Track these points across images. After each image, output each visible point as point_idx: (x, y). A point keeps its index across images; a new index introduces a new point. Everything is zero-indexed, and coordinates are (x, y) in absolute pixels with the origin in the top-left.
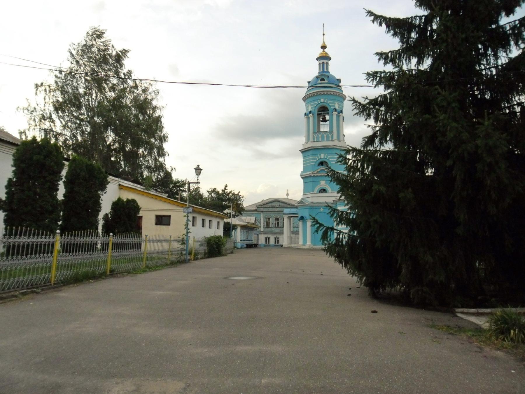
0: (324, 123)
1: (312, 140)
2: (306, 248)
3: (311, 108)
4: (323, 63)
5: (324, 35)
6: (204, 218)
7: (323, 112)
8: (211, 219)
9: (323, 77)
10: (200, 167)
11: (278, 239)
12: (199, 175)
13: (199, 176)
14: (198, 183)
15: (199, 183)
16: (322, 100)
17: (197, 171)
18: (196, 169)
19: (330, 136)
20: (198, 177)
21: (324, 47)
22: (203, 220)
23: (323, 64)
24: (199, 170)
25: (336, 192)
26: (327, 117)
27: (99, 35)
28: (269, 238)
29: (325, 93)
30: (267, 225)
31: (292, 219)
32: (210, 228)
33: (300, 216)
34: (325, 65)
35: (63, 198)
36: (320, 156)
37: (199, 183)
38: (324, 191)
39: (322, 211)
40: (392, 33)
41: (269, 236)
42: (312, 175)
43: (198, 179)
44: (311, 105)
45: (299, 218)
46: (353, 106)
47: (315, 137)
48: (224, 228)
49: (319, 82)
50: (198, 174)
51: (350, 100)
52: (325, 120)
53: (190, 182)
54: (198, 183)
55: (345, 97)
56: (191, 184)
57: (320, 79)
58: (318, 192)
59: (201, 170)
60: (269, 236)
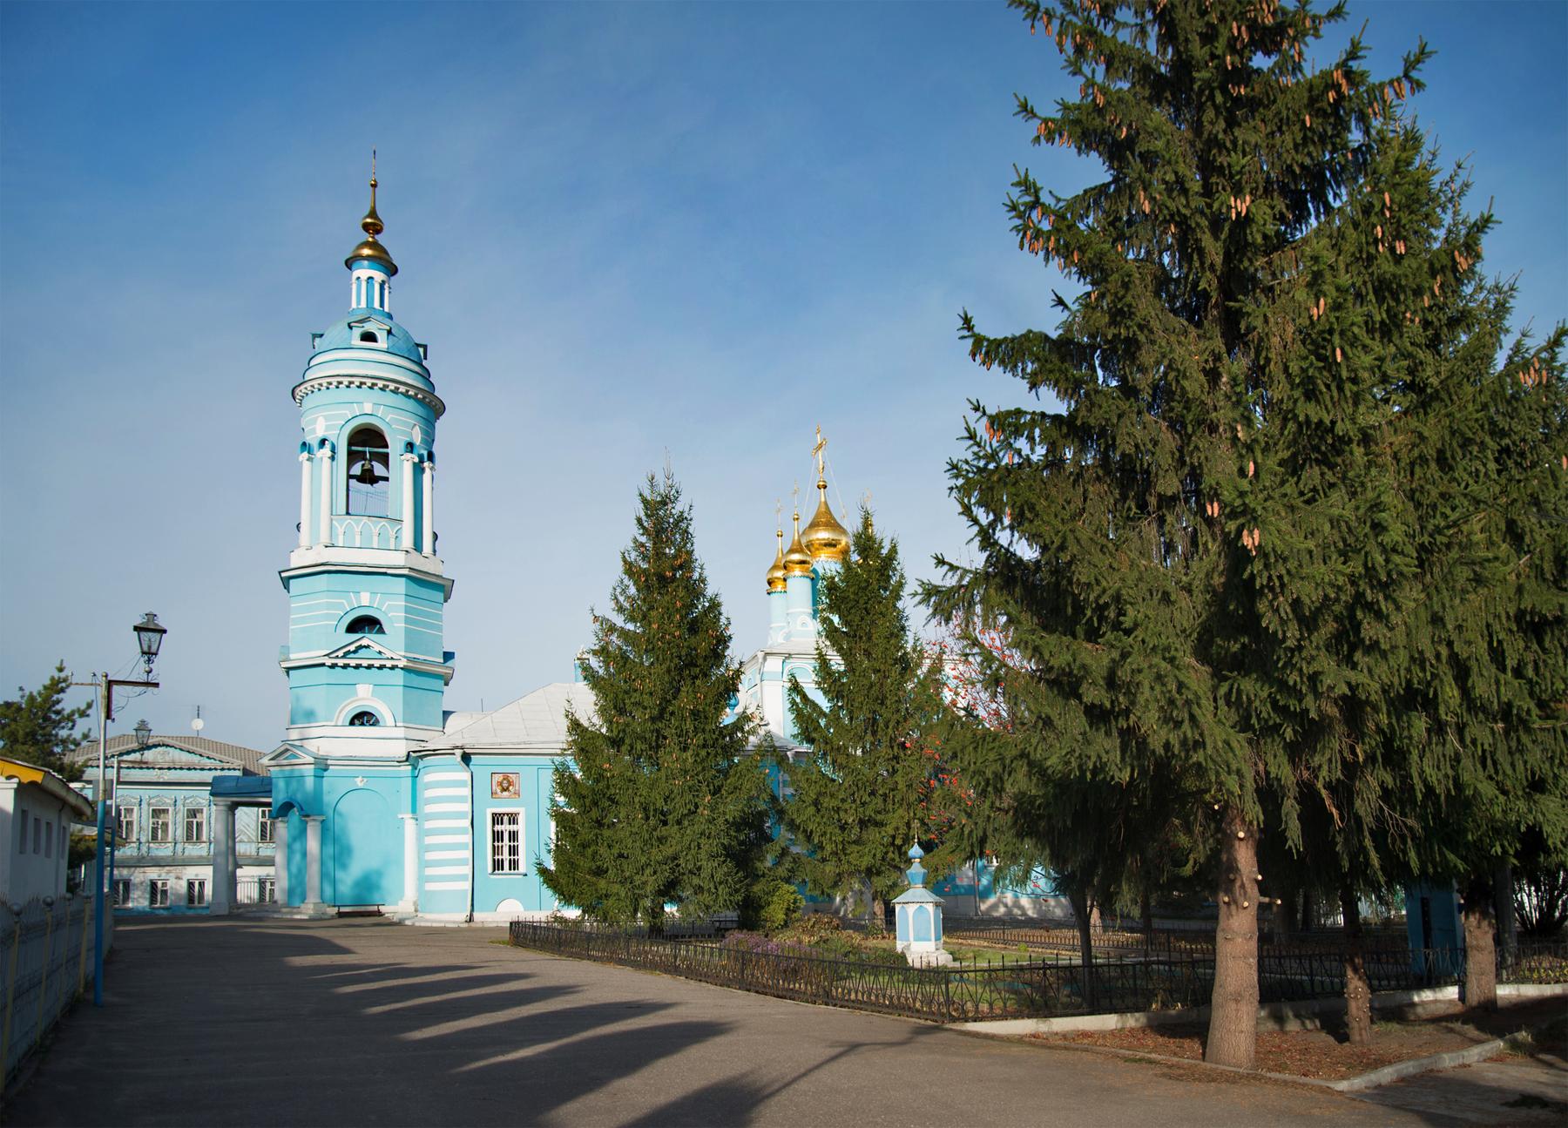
0: (367, 487)
2: (306, 917)
3: (327, 428)
5: (374, 186)
7: (367, 449)
9: (370, 327)
11: (272, 884)
13: (156, 659)
14: (147, 684)
15: (156, 685)
16: (368, 408)
19: (392, 534)
24: (157, 636)
26: (379, 470)
27: (1045, 723)
30: (263, 836)
36: (358, 600)
37: (156, 685)
38: (363, 718)
39: (360, 785)
40: (1113, 770)
44: (326, 418)
47: (340, 530)
49: (357, 342)
52: (368, 478)
53: (110, 678)
54: (147, 684)
56: (115, 688)
57: (357, 332)
58: (348, 723)
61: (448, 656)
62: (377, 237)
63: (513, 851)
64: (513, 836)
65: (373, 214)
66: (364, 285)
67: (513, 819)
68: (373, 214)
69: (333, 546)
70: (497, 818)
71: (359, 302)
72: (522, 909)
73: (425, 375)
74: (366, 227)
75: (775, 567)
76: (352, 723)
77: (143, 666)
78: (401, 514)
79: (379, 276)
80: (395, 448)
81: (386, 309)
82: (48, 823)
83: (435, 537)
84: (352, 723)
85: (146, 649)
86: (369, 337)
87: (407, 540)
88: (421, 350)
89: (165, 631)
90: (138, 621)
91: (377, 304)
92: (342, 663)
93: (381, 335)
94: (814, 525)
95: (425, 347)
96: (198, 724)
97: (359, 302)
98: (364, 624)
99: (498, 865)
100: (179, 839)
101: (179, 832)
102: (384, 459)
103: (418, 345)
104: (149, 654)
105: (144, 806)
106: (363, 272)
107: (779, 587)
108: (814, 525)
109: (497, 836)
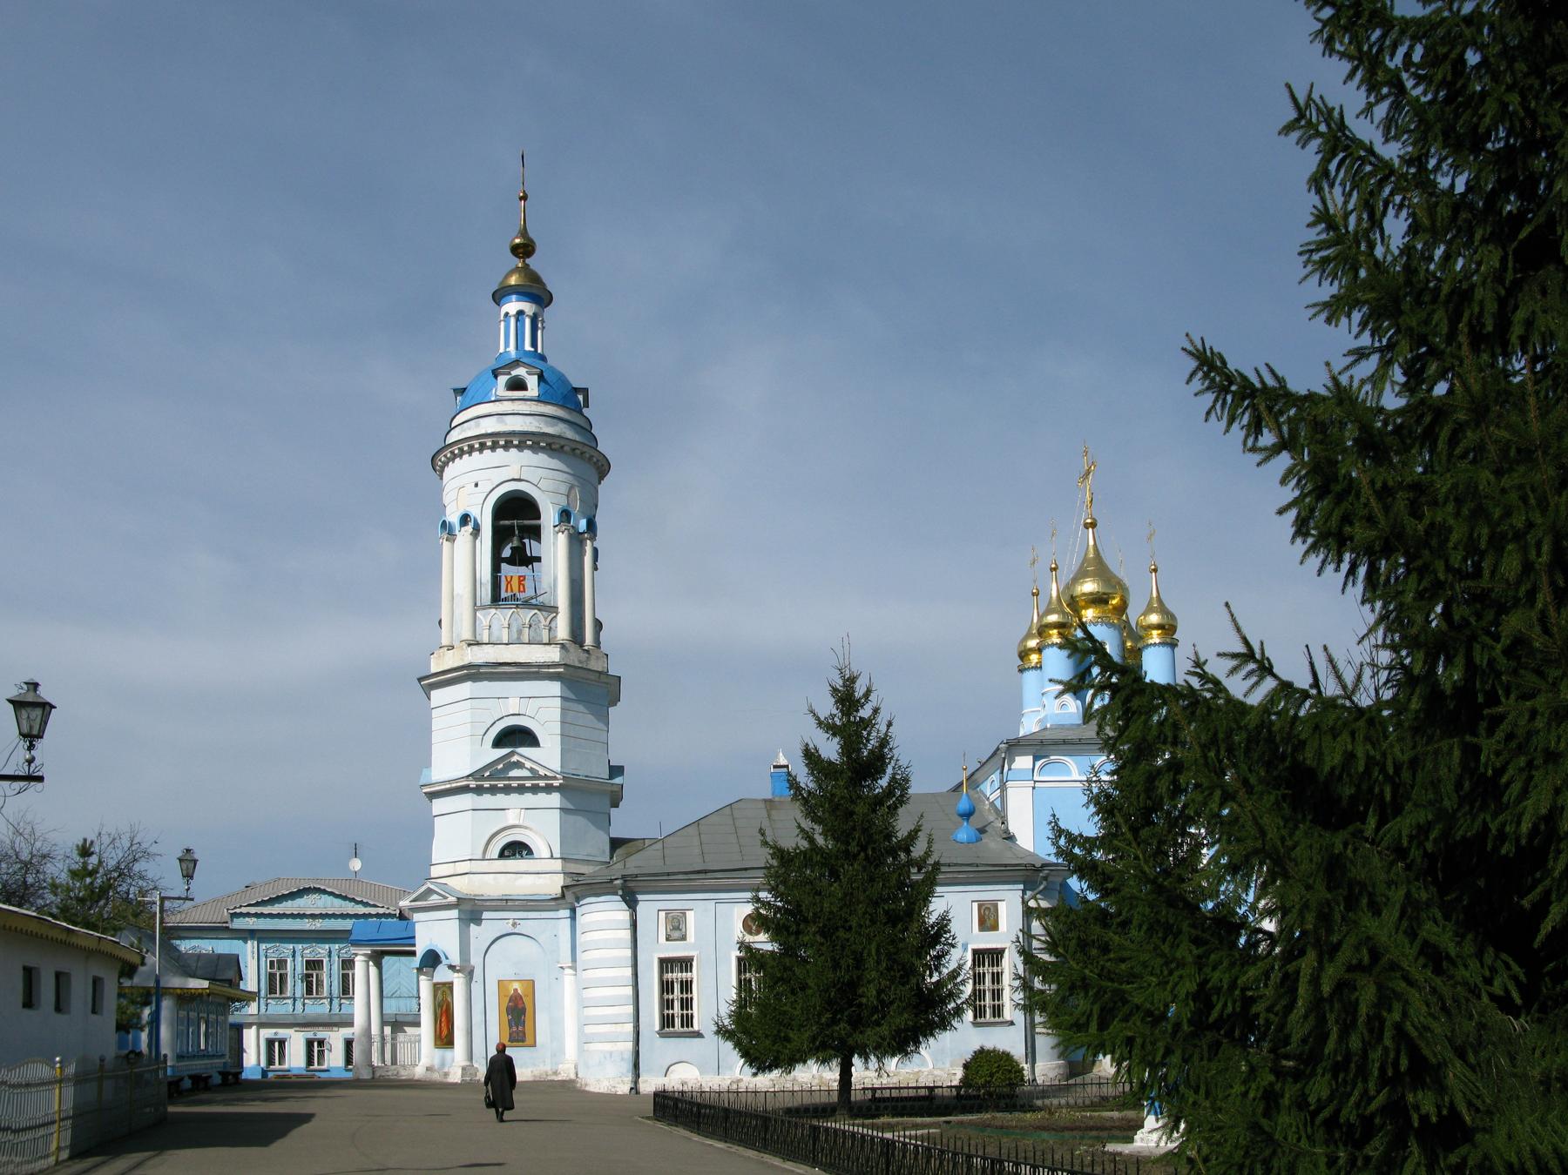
1: (467, 635)
4: (520, 313)
5: (524, 198)
6: (100, 974)
8: (63, 965)
9: (521, 372)
10: (45, 694)
12: (40, 736)
13: (39, 744)
15: (40, 779)
17: (24, 714)
18: (18, 704)
20: (31, 747)
21: (524, 250)
22: (97, 982)
23: (517, 320)
24: (38, 712)
25: (943, 869)
28: (282, 1042)
29: (489, 444)
31: (387, 960)
32: (58, 1009)
33: (420, 949)
34: (528, 322)
35: (1147, 680)
37: (40, 779)
38: (516, 849)
41: (321, 1034)
42: (473, 784)
43: (30, 761)
45: (416, 961)
46: (1257, 370)
48: (430, 755)
50: (31, 737)
51: (1315, 315)
55: (606, 464)
56: (549, 856)
59: (47, 707)
60: (282, 1033)
61: (616, 771)
62: (528, 261)
63: (687, 1004)
64: (687, 986)
65: (524, 233)
66: (513, 321)
67: (685, 963)
68: (524, 233)
69: (478, 644)
70: (666, 964)
71: (507, 344)
72: (697, 1073)
73: (585, 428)
74: (515, 250)
75: (1029, 636)
76: (502, 855)
77: (22, 754)
78: (555, 600)
79: (528, 308)
80: (549, 517)
81: (539, 351)
82: (58, 975)
83: (598, 625)
84: (502, 855)
85: (25, 730)
86: (517, 385)
87: (562, 630)
88: (581, 397)
89: (55, 707)
90: (13, 693)
91: (528, 347)
92: (486, 782)
93: (532, 382)
94: (1081, 575)
95: (585, 391)
96: (356, 865)
97: (507, 344)
98: (516, 736)
99: (667, 1021)
100: (298, 994)
101: (335, 984)
102: (535, 533)
103: (576, 390)
104: (31, 737)
105: (299, 959)
106: (512, 306)
107: (1034, 658)
108: (1081, 575)
109: (666, 987)
